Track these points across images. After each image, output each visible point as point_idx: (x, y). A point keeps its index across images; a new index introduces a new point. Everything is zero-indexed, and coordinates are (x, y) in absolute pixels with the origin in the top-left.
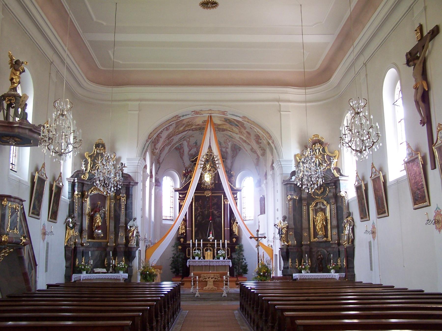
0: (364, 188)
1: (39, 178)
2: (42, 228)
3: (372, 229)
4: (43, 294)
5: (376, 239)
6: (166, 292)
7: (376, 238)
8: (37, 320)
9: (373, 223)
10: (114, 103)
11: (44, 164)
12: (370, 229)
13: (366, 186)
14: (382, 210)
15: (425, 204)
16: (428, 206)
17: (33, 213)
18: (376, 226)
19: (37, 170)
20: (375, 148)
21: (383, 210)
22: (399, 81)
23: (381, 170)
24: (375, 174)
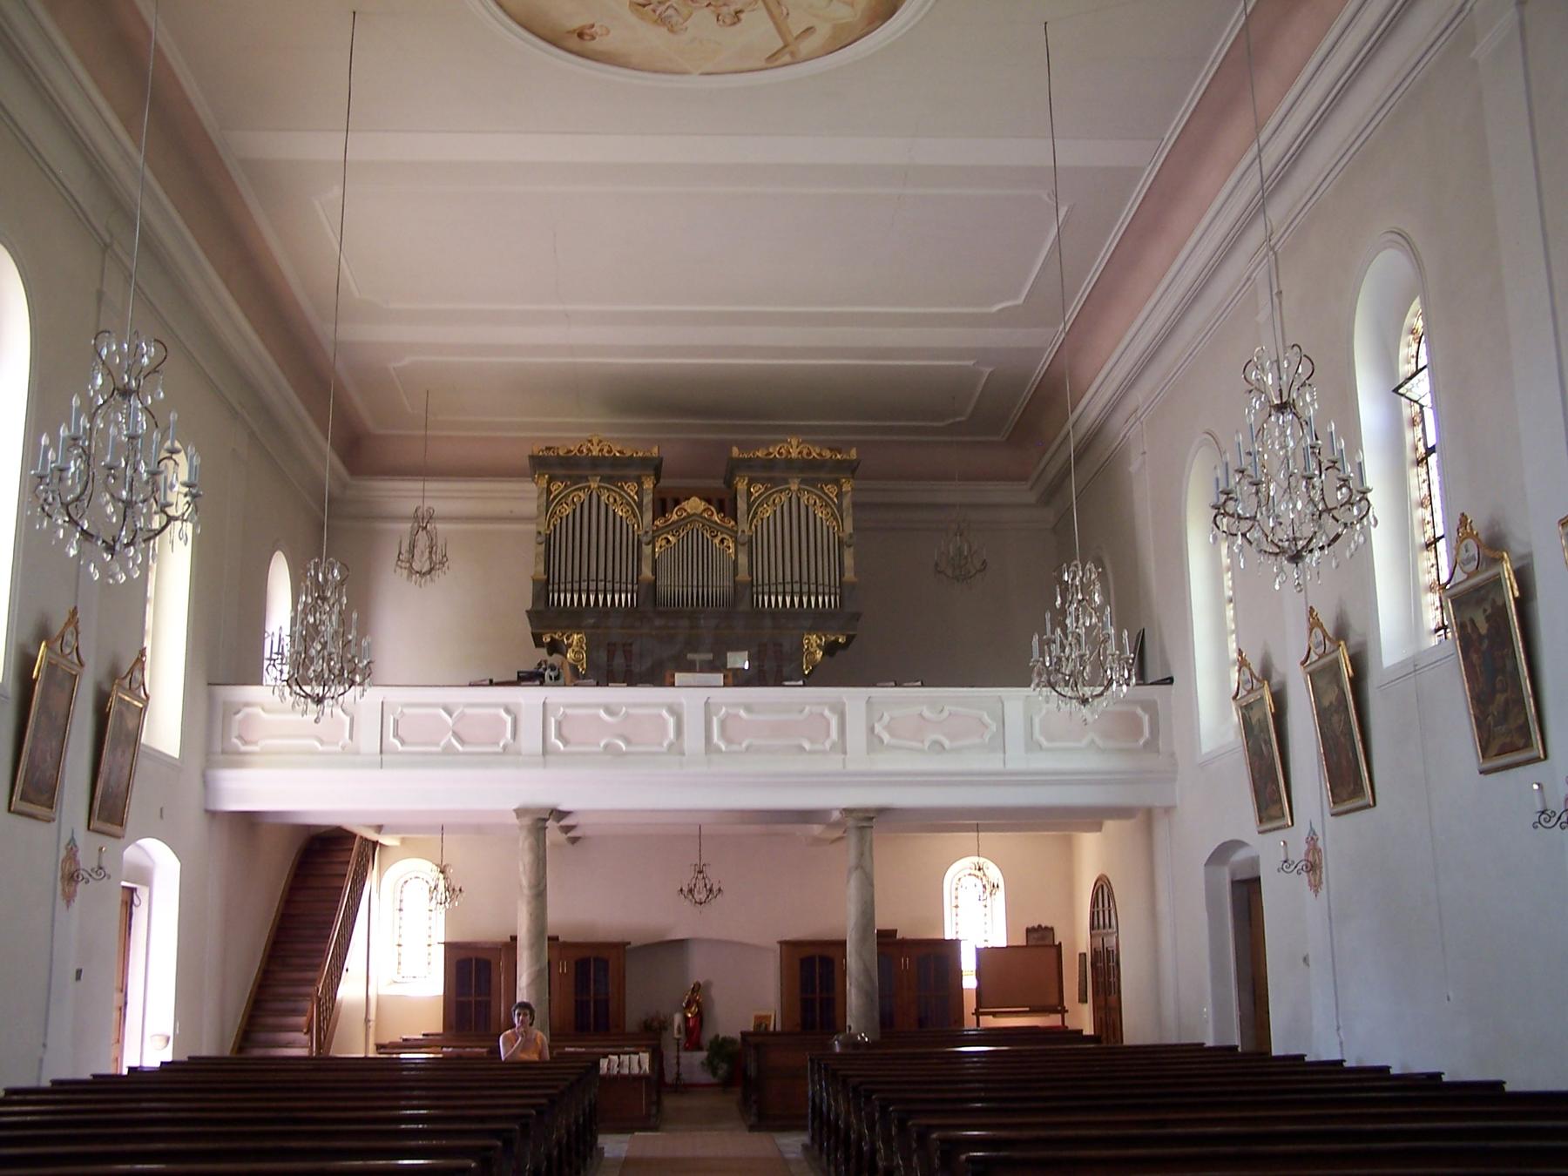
0: (1346, 671)
1: (51, 667)
2: (63, 853)
3: (1307, 854)
4: (1278, 1120)
5: (1323, 892)
6: (544, 1101)
7: (1324, 886)
8: (337, 1132)
9: (1312, 831)
10: (372, 1016)
11: (74, 612)
12: (1299, 852)
13: (1279, 699)
14: (1348, 779)
15: (1360, 802)
16: (1537, 760)
17: (23, 798)
18: (1320, 844)
19: (43, 634)
20: (1345, 549)
21: (1520, 721)
22: (1417, 300)
23: (1341, 633)
24: (1249, 687)
